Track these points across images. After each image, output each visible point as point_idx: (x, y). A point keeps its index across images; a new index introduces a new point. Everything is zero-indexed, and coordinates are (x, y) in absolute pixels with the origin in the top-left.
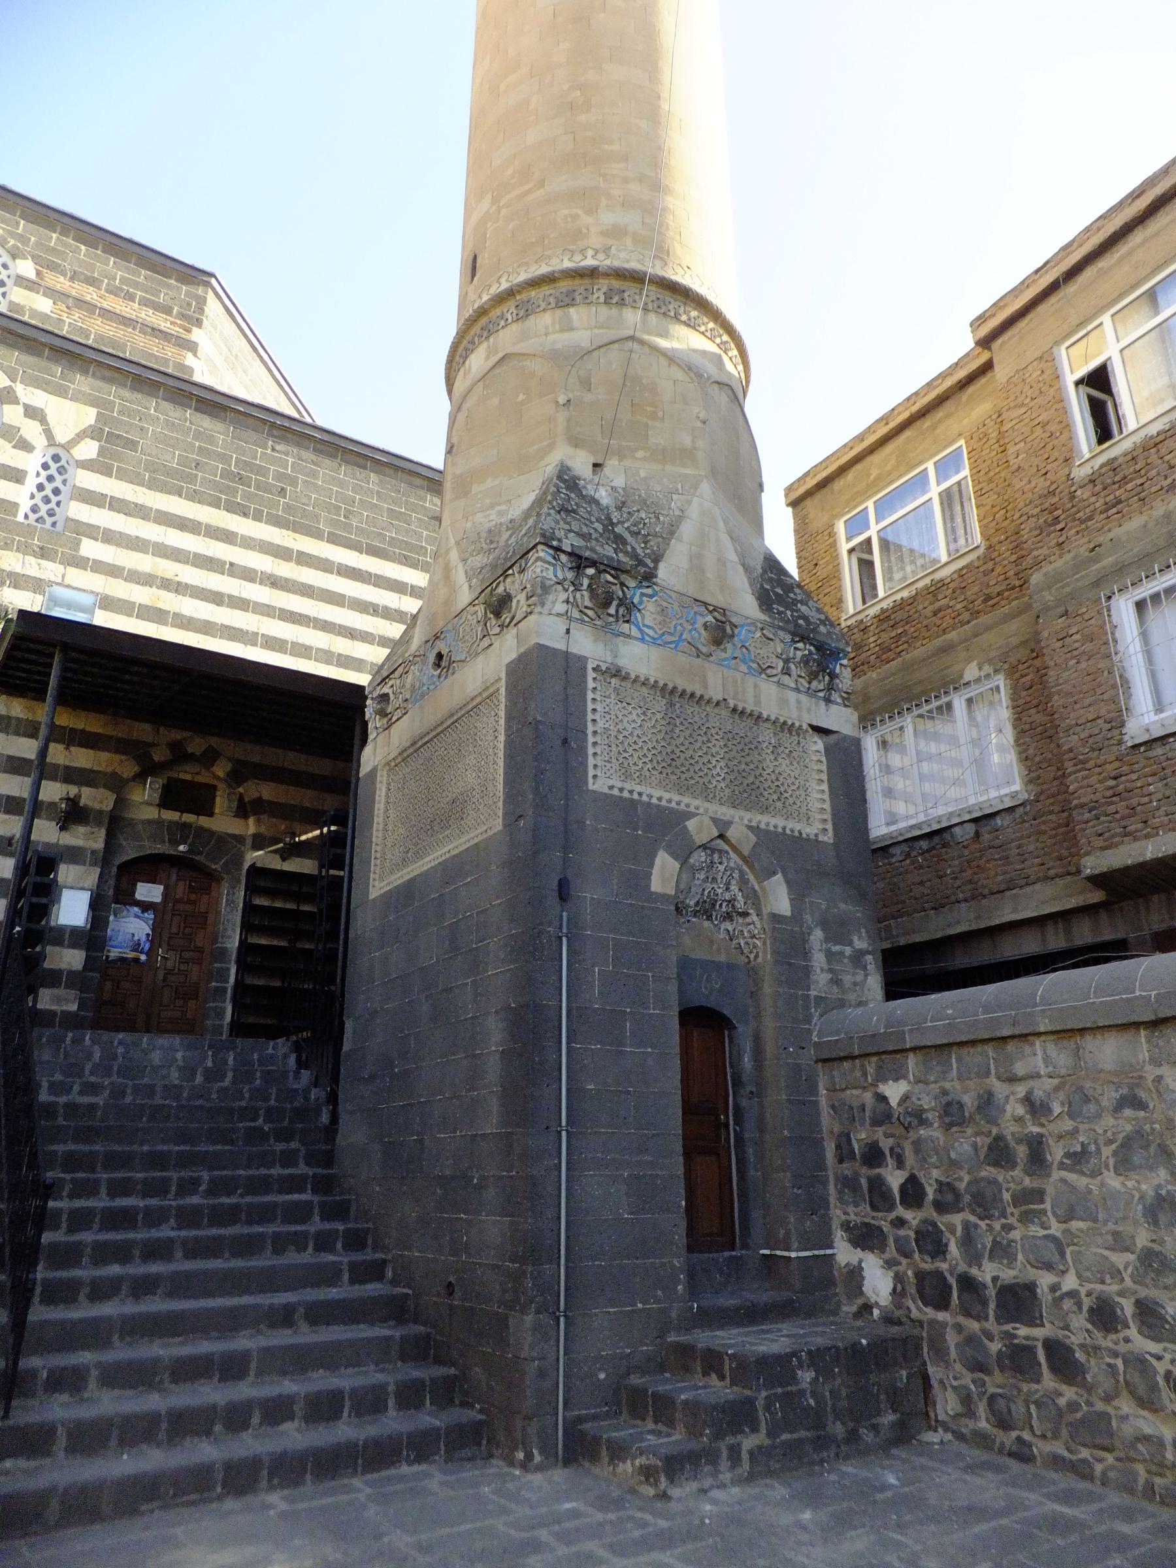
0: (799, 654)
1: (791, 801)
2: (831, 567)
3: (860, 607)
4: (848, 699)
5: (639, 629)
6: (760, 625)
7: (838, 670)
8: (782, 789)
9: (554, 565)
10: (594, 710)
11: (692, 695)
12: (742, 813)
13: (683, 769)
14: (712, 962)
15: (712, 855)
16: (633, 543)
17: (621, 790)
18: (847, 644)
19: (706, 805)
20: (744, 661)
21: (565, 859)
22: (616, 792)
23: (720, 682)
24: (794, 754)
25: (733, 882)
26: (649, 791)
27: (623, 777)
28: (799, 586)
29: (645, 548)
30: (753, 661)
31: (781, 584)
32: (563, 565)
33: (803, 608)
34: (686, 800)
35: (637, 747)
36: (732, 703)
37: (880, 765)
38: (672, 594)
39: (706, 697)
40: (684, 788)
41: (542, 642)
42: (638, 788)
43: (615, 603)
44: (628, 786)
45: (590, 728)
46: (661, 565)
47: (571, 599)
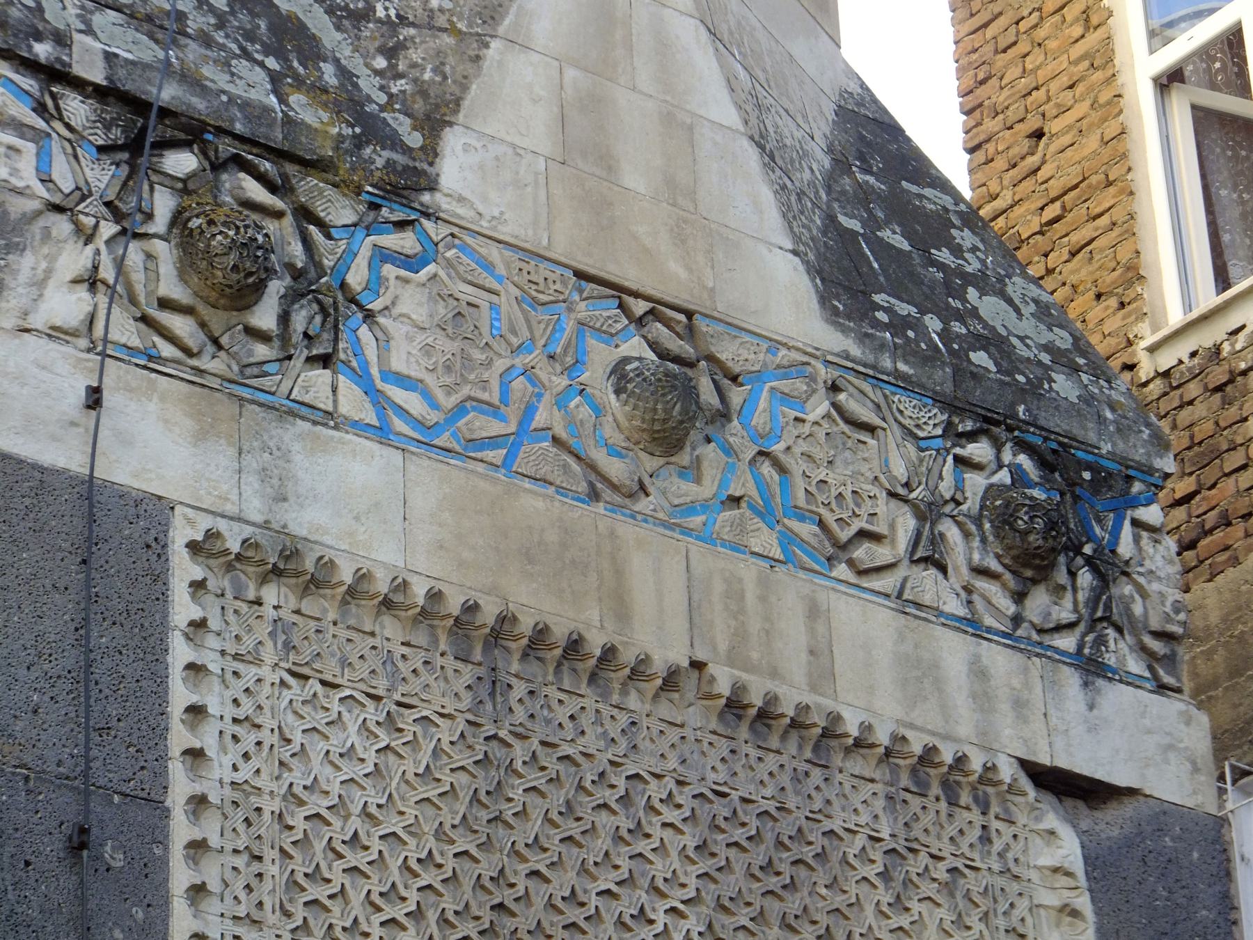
0: (976, 483)
2: (1092, 143)
3: (1207, 297)
4: (1170, 661)
5: (371, 391)
6: (824, 374)
7: (1125, 548)
9: (38, 137)
10: (196, 711)
16: (345, 52)
18: (1160, 443)
20: (765, 513)
23: (676, 598)
24: (972, 882)
28: (971, 218)
32: (75, 136)
33: (990, 307)
36: (723, 680)
38: (494, 253)
39: (628, 656)
43: (276, 288)
45: (180, 785)
46: (452, 141)
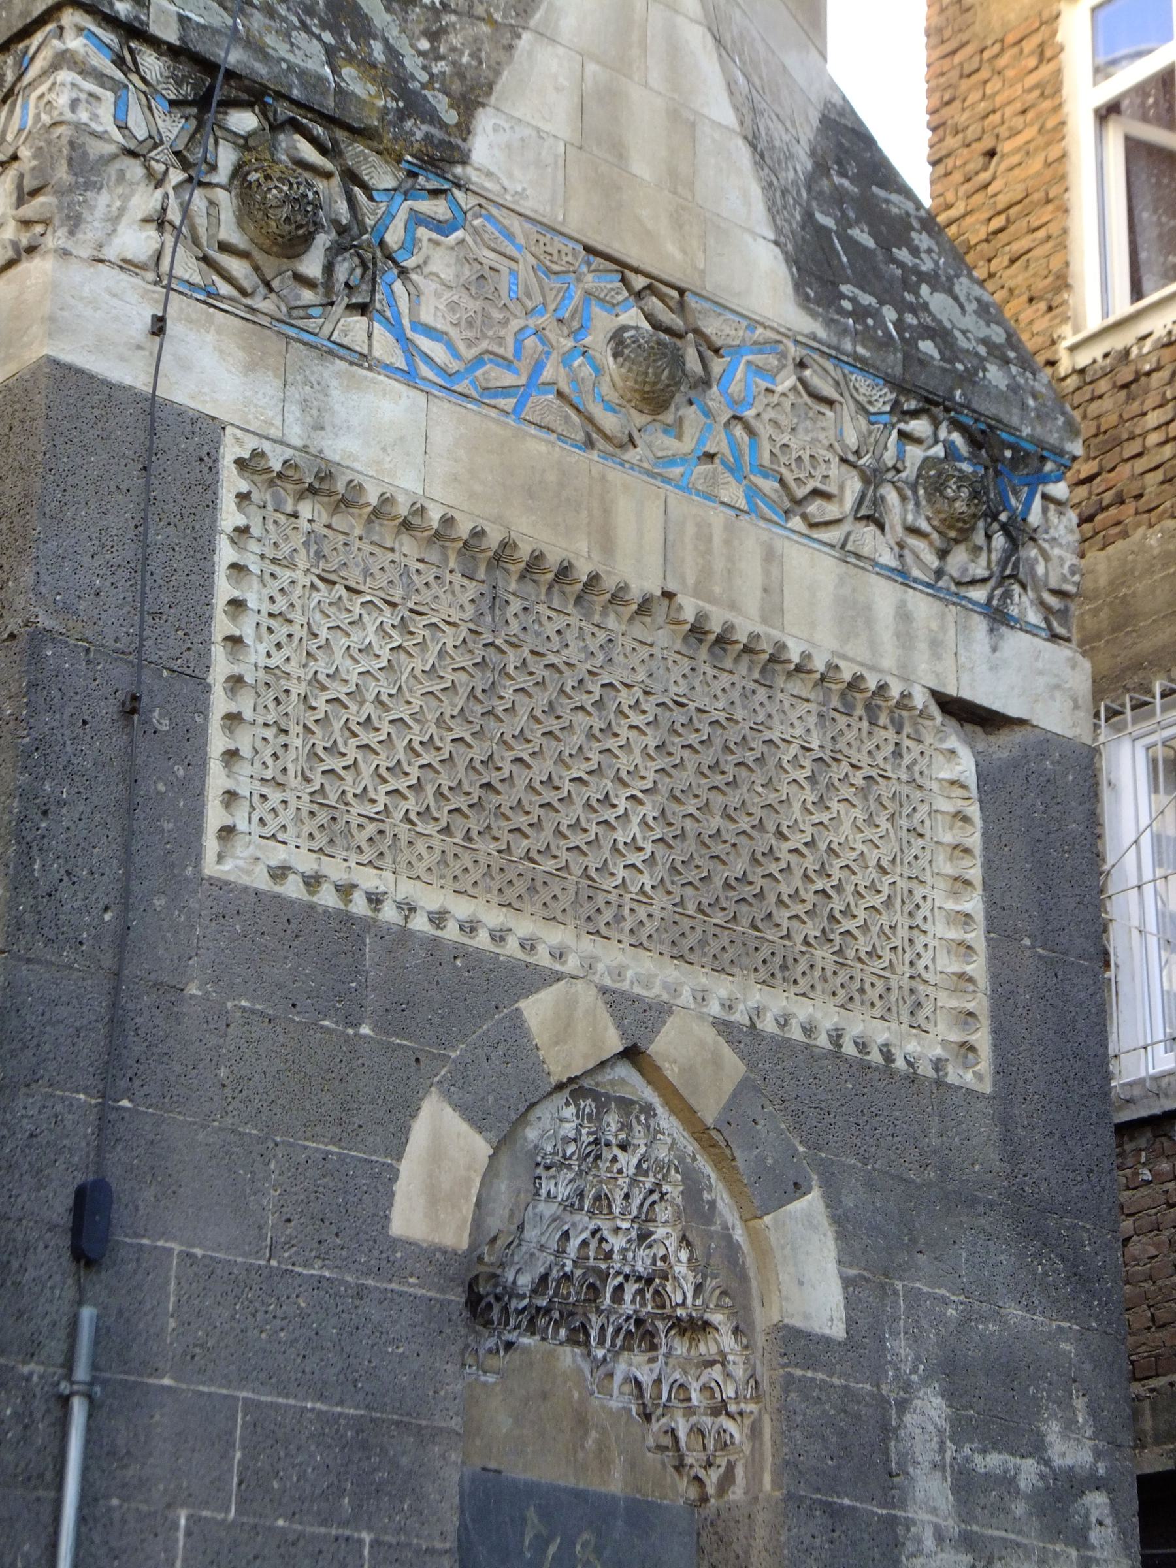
0: (915, 454)
1: (863, 944)
2: (1036, 164)
3: (1122, 306)
4: (1063, 615)
6: (793, 351)
7: (1035, 517)
8: (837, 905)
9: (117, 87)
10: (237, 604)
11: (564, 572)
12: (703, 978)
13: (521, 821)
14: (580, 1495)
15: (596, 1118)
16: (393, 33)
17: (313, 882)
18: (1072, 430)
19: (588, 945)
20: (735, 470)
21: (105, 1120)
22: (293, 889)
23: (653, 537)
24: (883, 789)
25: (664, 1213)
26: (406, 889)
27: (321, 840)
28: (929, 223)
29: (434, 55)
30: (765, 473)
31: (871, 213)
33: (938, 302)
34: (524, 927)
35: (371, 738)
36: (689, 609)
37: (1157, 840)
38: (515, 225)
39: (609, 584)
40: (521, 886)
41: (66, 357)
42: (368, 880)
43: (323, 240)
44: (335, 870)
45: (221, 666)
46: (484, 121)
47: (174, 215)
